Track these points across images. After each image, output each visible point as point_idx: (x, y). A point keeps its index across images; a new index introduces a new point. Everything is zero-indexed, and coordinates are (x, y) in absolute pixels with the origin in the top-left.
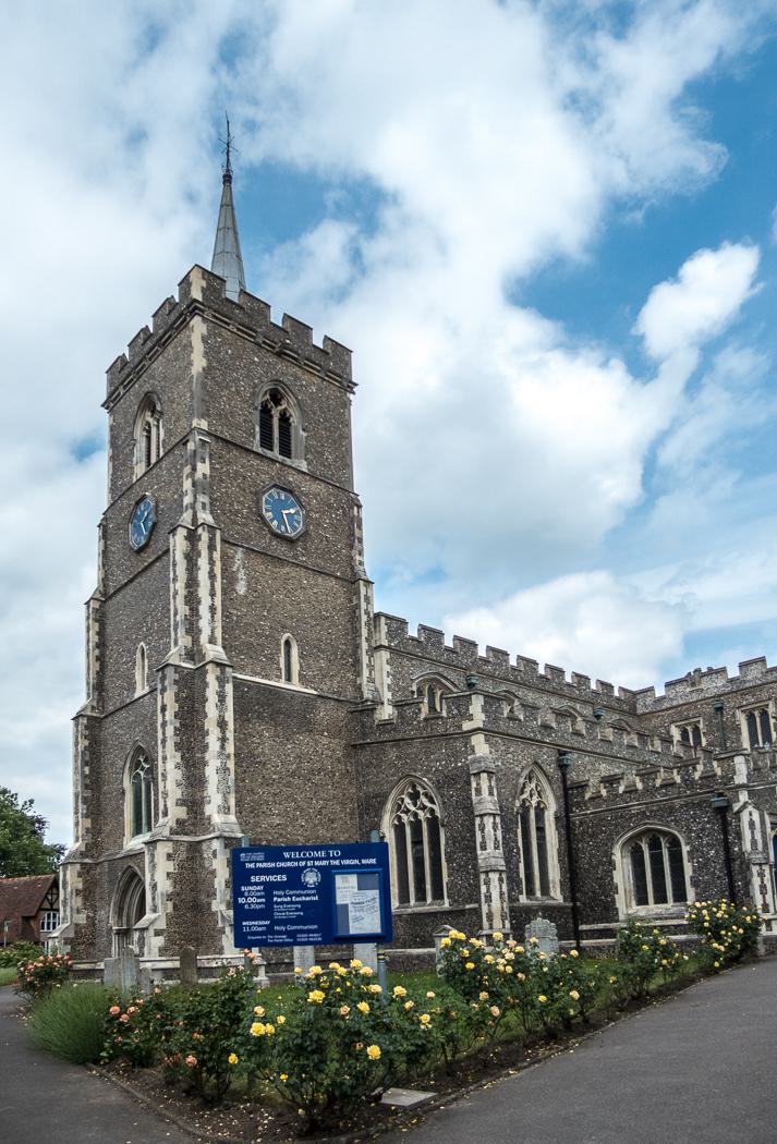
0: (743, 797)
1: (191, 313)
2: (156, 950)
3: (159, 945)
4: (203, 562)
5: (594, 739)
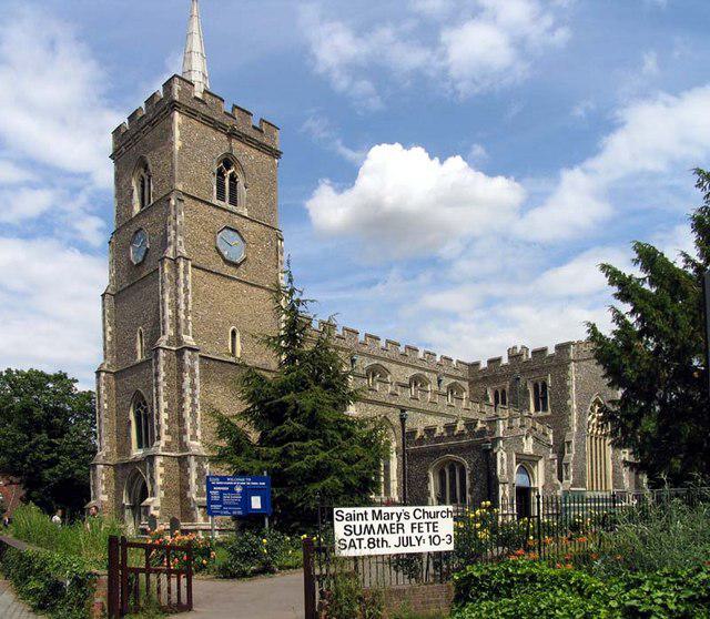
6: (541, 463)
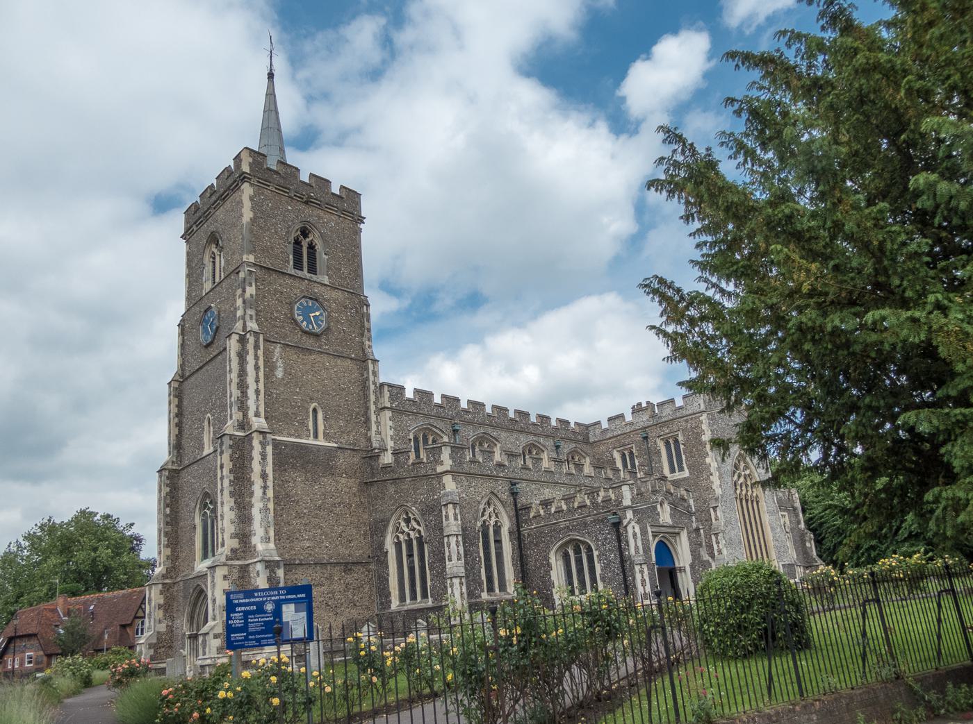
0: (630, 514)
1: (242, 180)
2: (215, 649)
3: (217, 645)
4: (250, 359)
5: (539, 470)
6: (684, 535)
